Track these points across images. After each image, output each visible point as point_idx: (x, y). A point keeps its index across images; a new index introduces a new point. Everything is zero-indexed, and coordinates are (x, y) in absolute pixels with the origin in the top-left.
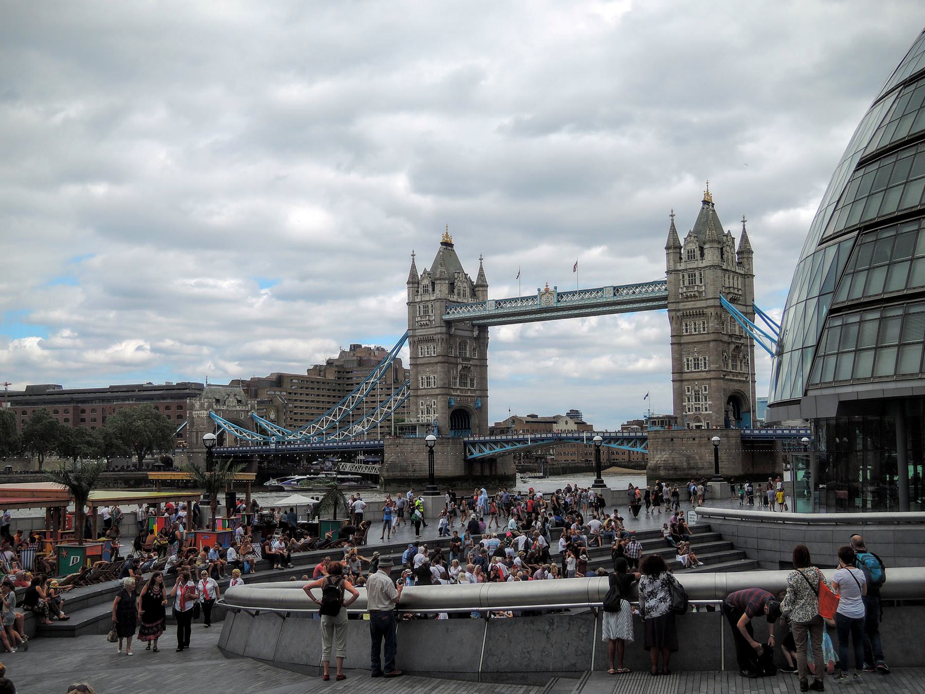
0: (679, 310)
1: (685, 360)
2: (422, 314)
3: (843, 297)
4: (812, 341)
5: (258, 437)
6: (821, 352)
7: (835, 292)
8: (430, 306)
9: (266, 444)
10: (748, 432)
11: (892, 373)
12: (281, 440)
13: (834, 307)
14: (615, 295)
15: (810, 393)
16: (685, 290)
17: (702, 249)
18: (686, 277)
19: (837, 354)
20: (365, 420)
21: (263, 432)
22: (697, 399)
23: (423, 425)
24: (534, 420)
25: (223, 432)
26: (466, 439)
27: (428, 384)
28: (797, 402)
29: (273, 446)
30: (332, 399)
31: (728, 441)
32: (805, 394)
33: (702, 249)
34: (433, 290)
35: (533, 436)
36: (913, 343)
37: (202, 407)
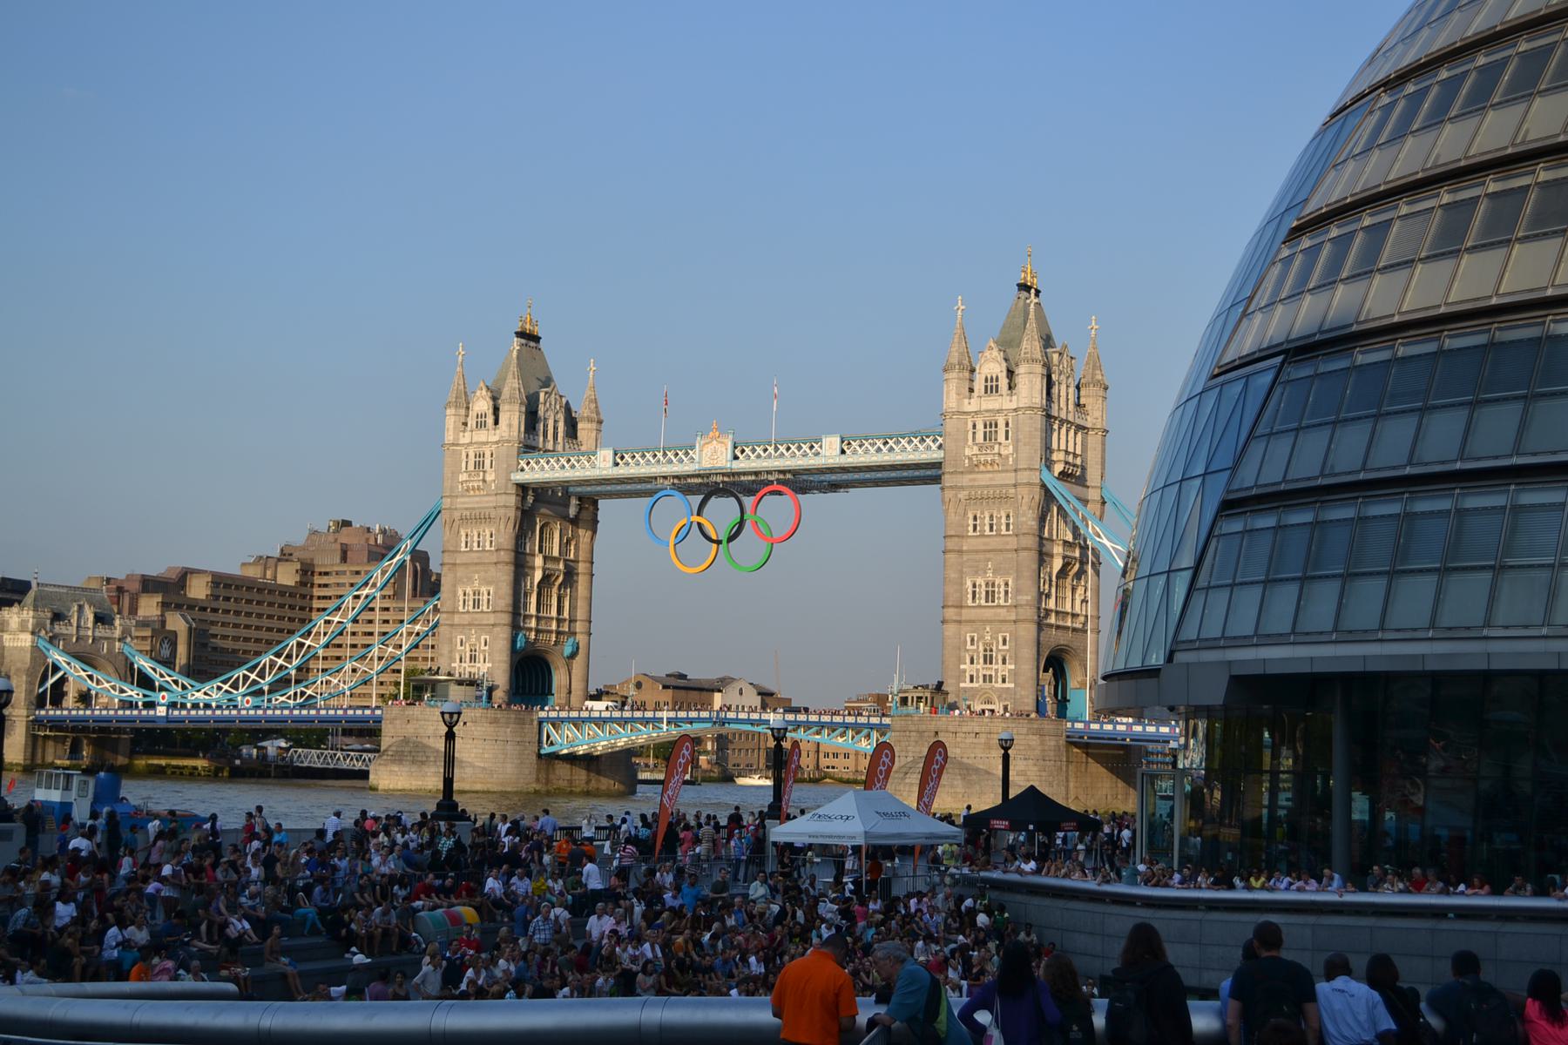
0: (962, 488)
1: (969, 584)
2: (471, 467)
3: (1248, 478)
4: (1187, 559)
5: (134, 693)
6: (1202, 581)
7: (1234, 469)
8: (488, 454)
9: (150, 705)
10: (1079, 726)
11: (1330, 628)
12: (180, 700)
13: (1232, 496)
14: (843, 452)
15: (1180, 657)
16: (976, 450)
17: (496, 410)
18: (980, 426)
19: (1232, 586)
20: (348, 666)
21: (145, 682)
22: (988, 660)
23: (460, 683)
24: (681, 682)
25: (63, 680)
26: (542, 714)
27: (477, 603)
28: (1153, 673)
29: (161, 711)
30: (275, 624)
31: (1042, 743)
32: (1170, 659)
33: (1010, 373)
34: (496, 422)
35: (672, 714)
36: (1371, 574)
37: (23, 629)
